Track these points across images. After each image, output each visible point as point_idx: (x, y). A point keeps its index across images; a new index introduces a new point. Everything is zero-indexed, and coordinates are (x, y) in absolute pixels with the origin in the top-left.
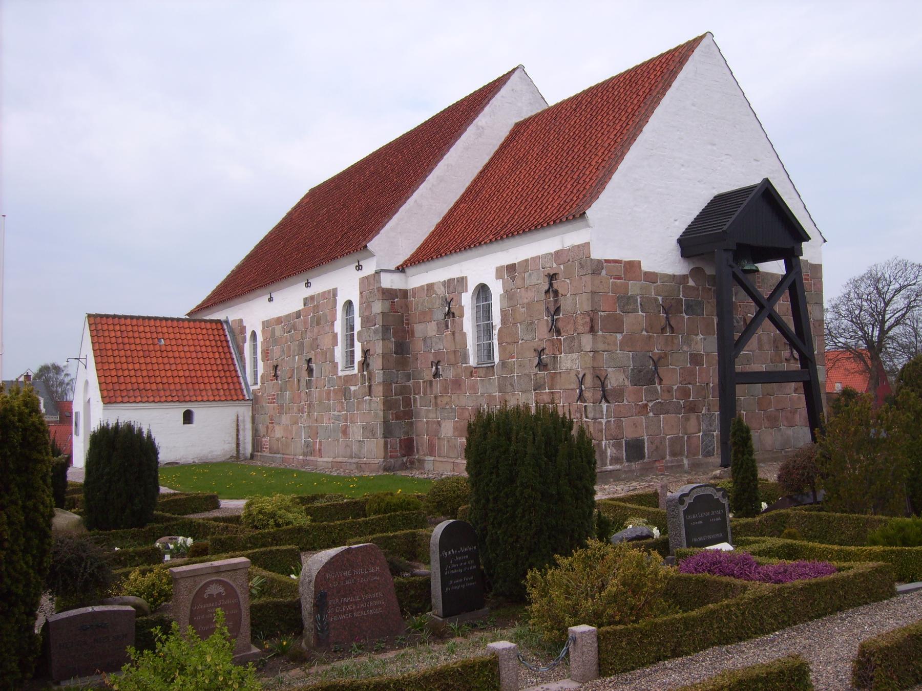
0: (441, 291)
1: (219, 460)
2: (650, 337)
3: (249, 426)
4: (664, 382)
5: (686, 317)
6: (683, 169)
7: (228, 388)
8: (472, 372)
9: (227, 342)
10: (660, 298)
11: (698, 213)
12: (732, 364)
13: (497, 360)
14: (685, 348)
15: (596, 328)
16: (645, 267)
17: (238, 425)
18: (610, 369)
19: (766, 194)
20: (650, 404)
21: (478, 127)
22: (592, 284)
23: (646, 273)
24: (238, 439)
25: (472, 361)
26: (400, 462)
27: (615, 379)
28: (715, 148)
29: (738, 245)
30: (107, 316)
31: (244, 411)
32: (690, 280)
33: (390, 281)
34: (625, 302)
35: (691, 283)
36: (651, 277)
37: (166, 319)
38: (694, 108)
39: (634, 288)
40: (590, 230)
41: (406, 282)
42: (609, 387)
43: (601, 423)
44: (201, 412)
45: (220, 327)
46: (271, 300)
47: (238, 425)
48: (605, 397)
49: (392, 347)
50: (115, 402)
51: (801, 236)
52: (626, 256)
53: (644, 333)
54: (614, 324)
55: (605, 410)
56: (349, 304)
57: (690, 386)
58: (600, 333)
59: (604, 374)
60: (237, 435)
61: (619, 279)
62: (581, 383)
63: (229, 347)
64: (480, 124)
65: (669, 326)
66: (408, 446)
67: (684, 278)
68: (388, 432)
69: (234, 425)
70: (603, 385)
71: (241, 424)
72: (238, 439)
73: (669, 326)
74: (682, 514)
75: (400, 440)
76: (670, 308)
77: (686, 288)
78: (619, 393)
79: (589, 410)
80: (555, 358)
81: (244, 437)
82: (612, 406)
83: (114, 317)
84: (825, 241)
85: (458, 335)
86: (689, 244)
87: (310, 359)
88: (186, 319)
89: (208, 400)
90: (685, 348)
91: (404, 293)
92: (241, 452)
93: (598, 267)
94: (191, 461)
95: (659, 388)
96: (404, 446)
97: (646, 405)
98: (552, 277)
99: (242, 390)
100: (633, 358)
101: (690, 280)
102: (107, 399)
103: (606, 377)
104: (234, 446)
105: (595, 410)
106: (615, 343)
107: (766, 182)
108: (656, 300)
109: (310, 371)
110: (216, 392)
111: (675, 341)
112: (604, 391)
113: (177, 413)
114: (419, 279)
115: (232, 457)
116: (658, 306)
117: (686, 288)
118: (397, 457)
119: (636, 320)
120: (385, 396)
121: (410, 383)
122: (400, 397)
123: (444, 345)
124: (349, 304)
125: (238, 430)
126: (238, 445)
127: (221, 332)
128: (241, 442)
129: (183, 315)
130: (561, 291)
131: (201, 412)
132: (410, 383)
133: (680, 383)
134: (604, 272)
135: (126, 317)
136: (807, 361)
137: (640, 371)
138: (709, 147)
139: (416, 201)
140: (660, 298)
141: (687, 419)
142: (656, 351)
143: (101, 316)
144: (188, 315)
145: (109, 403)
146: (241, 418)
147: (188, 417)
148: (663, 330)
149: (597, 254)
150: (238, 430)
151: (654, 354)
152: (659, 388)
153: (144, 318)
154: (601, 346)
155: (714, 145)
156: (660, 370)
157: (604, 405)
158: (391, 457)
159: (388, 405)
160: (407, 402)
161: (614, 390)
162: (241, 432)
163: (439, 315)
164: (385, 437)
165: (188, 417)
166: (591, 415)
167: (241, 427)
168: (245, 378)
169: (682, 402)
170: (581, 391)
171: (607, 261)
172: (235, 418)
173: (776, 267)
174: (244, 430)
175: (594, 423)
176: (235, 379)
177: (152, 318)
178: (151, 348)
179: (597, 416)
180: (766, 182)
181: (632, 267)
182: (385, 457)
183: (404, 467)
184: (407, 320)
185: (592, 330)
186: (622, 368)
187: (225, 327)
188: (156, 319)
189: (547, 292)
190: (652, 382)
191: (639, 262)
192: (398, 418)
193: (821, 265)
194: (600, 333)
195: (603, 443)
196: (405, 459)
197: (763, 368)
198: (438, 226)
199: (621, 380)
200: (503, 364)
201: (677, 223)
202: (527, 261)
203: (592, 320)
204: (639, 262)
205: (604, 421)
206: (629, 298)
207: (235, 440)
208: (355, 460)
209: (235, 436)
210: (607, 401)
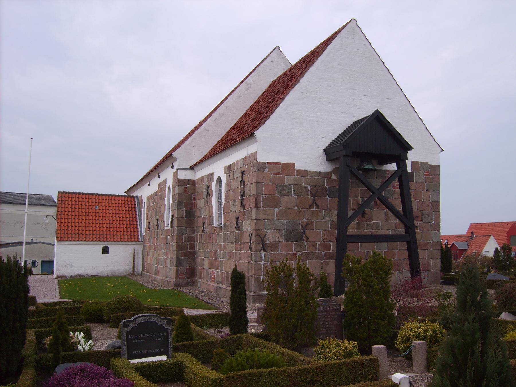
0: (206, 180)
1: (122, 275)
2: (300, 211)
3: (141, 256)
4: (310, 239)
5: (329, 198)
6: (330, 105)
7: (129, 233)
8: (215, 229)
9: (135, 208)
10: (309, 187)
11: (341, 133)
12: (346, 229)
13: (223, 223)
14: (327, 218)
15: (259, 205)
16: (298, 167)
17: (134, 256)
18: (268, 231)
19: (378, 119)
20: (299, 254)
21: (247, 84)
22: (258, 177)
23: (298, 171)
24: (134, 263)
25: (215, 224)
26: (185, 281)
27: (271, 237)
28: (355, 91)
29: (354, 153)
30: (69, 193)
31: (138, 248)
32: (333, 175)
33: (183, 175)
34: (283, 189)
35: (334, 177)
36: (303, 173)
37: (102, 195)
38: (340, 67)
39: (288, 180)
40: (257, 144)
41: (194, 176)
42: (267, 242)
43: (260, 265)
44: (113, 248)
45: (132, 200)
46: (149, 185)
47: (134, 256)
48: (264, 248)
49: (184, 213)
50: (64, 240)
51: (406, 147)
52: (284, 160)
53: (296, 208)
54: (273, 203)
55: (263, 256)
56: (169, 187)
57: (331, 243)
58: (262, 208)
59: (264, 234)
60: (134, 261)
61: (278, 174)
62: (251, 239)
63: (136, 211)
64: (249, 82)
65: (314, 204)
66: (192, 273)
67: (328, 174)
68: (179, 263)
69: (133, 255)
70: (263, 241)
71: (136, 255)
72: (134, 263)
73: (314, 204)
74: (125, 334)
75: (187, 269)
76: (317, 193)
77: (330, 181)
78: (275, 246)
79: (253, 256)
80: (242, 222)
81: (138, 262)
82: (269, 254)
83: (73, 193)
84: (443, 150)
85: (210, 207)
86: (330, 153)
87: (238, 217)
88: (125, 196)
89: (117, 241)
90: (327, 218)
91: (193, 182)
92: (136, 271)
93: (262, 167)
94: (106, 275)
95: (306, 243)
96: (188, 271)
97: (296, 254)
98: (243, 173)
99: (138, 235)
100: (286, 224)
101: (333, 175)
102: (59, 239)
103: (265, 235)
104: (132, 267)
105: (256, 256)
106: (273, 214)
107: (377, 112)
108: (306, 188)
109: (158, 225)
110: (122, 237)
111: (320, 214)
112: (263, 244)
113: (99, 247)
114: (202, 173)
115: (130, 273)
116: (307, 191)
117: (330, 181)
118: (184, 279)
119: (290, 200)
120: (178, 243)
121: (194, 235)
122: (188, 243)
123: (205, 214)
124: (169, 187)
125: (134, 259)
126: (134, 267)
127: (133, 203)
128: (136, 265)
129: (122, 193)
130: (246, 182)
131: (113, 248)
132: (194, 235)
133: (323, 240)
134: (266, 170)
135: (79, 194)
136: (410, 229)
137: (291, 233)
138: (351, 91)
139: (205, 128)
140: (309, 187)
141: (327, 264)
142: (304, 220)
143: (66, 193)
144: (126, 192)
145: (60, 241)
146: (136, 252)
147: (106, 250)
148: (310, 206)
149: (261, 158)
150: (134, 259)
151: (303, 222)
152: (306, 243)
153: (90, 194)
154: (262, 216)
155: (355, 89)
156: (308, 232)
157: (263, 254)
158: (180, 278)
159: (179, 247)
160: (192, 247)
161: (271, 244)
162: (136, 260)
163: (205, 195)
164: (177, 266)
165: (106, 250)
166: (254, 259)
167: (136, 257)
168: (141, 229)
169: (323, 253)
170: (251, 244)
171: (268, 163)
172: (133, 251)
173: (393, 167)
174: (138, 258)
175: (255, 264)
176: (135, 229)
177: (94, 194)
178: (91, 211)
179: (258, 260)
180: (377, 112)
181: (288, 168)
182: (176, 278)
183: (188, 284)
184: (194, 198)
185: (257, 206)
186: (278, 230)
187: (136, 200)
188: (96, 195)
189: (241, 182)
190: (301, 239)
191: (294, 164)
192: (185, 255)
193: (438, 167)
194: (262, 208)
195: (262, 277)
196: (189, 280)
197: (390, 232)
198: (219, 142)
199: (277, 238)
200: (225, 225)
201: (324, 139)
202: (234, 163)
203: (256, 200)
204: (294, 164)
205: (262, 263)
206: (285, 186)
207: (132, 264)
208: (167, 279)
209: (132, 261)
210: (265, 251)
